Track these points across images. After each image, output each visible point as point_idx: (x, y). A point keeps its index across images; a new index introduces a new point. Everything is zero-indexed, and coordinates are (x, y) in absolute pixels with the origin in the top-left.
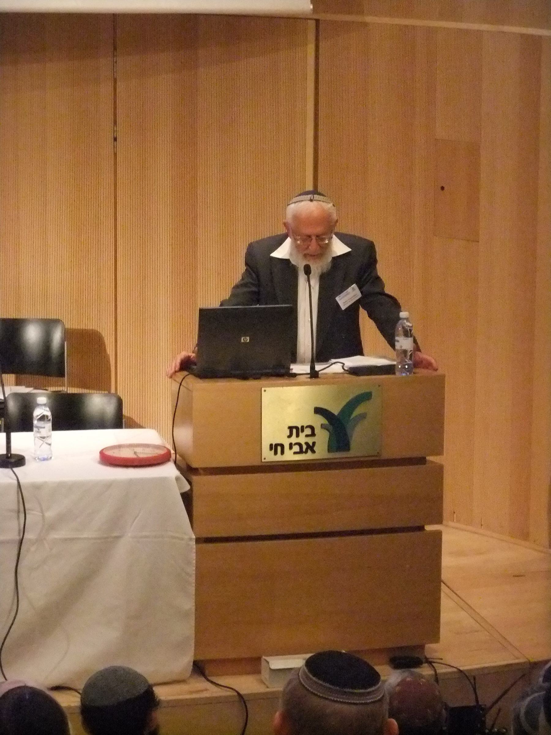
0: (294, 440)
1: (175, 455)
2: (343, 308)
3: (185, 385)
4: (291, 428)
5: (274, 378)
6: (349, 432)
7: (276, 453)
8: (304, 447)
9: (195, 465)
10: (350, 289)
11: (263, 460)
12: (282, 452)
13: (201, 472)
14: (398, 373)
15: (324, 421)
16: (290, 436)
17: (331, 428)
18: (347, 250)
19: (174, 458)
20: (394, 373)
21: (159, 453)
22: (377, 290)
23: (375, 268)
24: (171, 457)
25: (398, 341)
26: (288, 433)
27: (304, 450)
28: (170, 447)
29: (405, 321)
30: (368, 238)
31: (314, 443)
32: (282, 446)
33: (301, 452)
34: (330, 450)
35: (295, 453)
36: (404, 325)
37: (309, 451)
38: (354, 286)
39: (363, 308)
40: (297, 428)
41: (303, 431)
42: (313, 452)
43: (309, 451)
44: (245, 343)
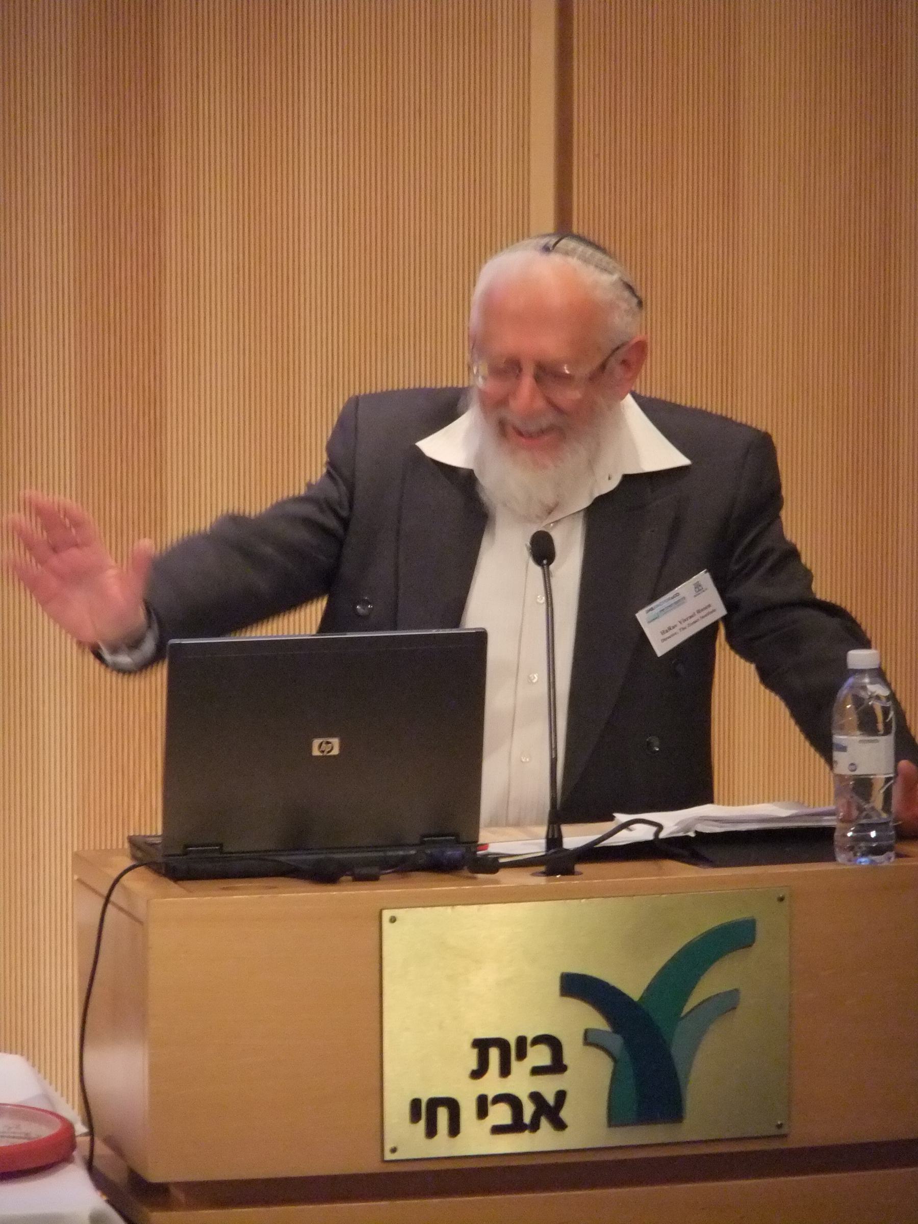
0: (492, 1085)
1: (88, 1139)
2: (661, 648)
3: (123, 903)
4: (482, 1046)
5: (422, 876)
6: (677, 1051)
7: (431, 1131)
8: (529, 1110)
9: (156, 1174)
10: (684, 589)
11: (389, 1156)
12: (454, 1129)
13: (182, 1197)
14: (843, 856)
15: (597, 1021)
16: (478, 1073)
17: (617, 1042)
18: (675, 459)
19: (87, 1153)
20: (832, 858)
21: (33, 1135)
22: (793, 592)
23: (776, 517)
24: (73, 1146)
25: (843, 749)
26: (471, 1061)
27: (527, 1119)
28: (72, 1113)
29: (867, 680)
30: (742, 416)
31: (561, 1096)
32: (453, 1106)
33: (517, 1126)
34: (615, 1118)
35: (498, 1130)
36: (863, 694)
37: (544, 1123)
38: (704, 578)
39: (732, 647)
40: (502, 1044)
41: (521, 1055)
42: (559, 1125)
43: (544, 1123)
44: (326, 760)
